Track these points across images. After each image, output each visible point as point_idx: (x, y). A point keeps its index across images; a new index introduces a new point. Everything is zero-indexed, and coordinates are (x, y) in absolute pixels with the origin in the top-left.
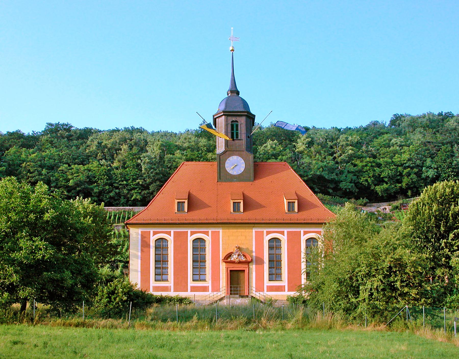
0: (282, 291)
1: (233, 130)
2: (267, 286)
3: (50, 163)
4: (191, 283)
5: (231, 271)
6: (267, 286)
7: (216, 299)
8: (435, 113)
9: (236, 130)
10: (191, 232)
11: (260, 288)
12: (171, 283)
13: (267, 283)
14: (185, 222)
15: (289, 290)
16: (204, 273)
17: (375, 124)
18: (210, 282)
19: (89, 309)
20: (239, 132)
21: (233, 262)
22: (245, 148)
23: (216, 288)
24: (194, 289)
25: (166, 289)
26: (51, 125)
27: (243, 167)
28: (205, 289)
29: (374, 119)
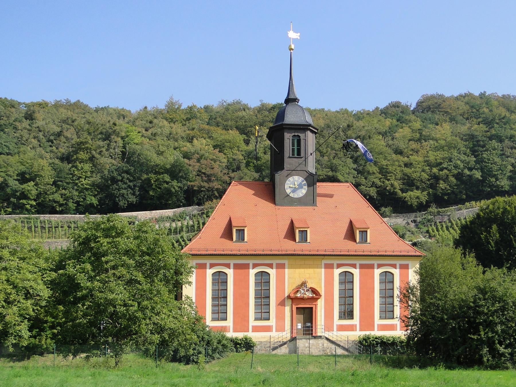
0: (353, 330)
1: (297, 148)
5: (312, 308)
7: (285, 340)
9: (292, 146)
10: (337, 264)
11: (329, 327)
12: (229, 323)
13: (337, 321)
15: (361, 330)
16: (382, 305)
17: (238, 103)
18: (274, 320)
20: (291, 147)
21: (302, 299)
22: (337, 176)
23: (280, 328)
24: (256, 329)
26: (79, 101)
28: (268, 329)
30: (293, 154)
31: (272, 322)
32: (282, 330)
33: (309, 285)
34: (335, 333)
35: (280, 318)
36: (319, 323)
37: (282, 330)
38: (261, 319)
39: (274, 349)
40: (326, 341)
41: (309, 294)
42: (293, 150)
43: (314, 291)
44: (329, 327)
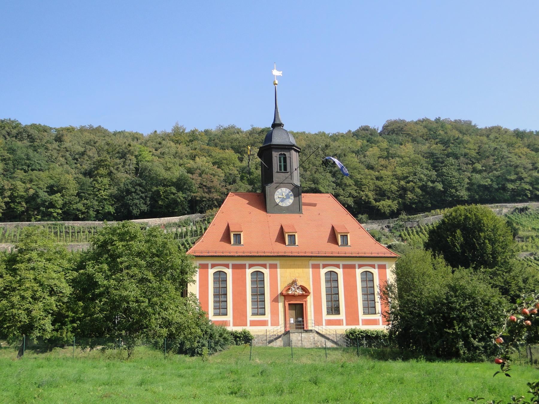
0: (340, 325)
2: (250, 321)
3: (191, 183)
4: (250, 317)
5: (302, 304)
6: (250, 321)
8: (371, 126)
11: (318, 322)
12: (229, 317)
13: (325, 317)
14: (256, 254)
15: (347, 324)
16: (364, 302)
18: (269, 315)
19: (147, 336)
21: (293, 296)
23: (275, 323)
24: (253, 323)
25: (375, 322)
27: (282, 190)
28: (264, 323)
29: (364, 124)
30: (280, 170)
31: (267, 317)
32: (277, 324)
33: (299, 283)
34: (324, 327)
35: (275, 313)
36: (309, 318)
37: (277, 324)
38: (257, 314)
39: (270, 342)
40: (316, 335)
41: (300, 292)
42: (280, 166)
43: (303, 289)
44: (318, 322)
